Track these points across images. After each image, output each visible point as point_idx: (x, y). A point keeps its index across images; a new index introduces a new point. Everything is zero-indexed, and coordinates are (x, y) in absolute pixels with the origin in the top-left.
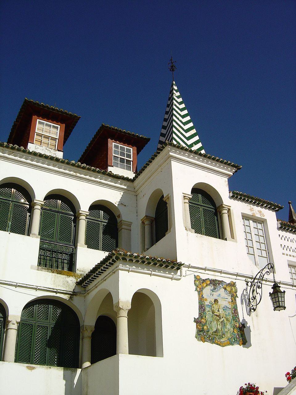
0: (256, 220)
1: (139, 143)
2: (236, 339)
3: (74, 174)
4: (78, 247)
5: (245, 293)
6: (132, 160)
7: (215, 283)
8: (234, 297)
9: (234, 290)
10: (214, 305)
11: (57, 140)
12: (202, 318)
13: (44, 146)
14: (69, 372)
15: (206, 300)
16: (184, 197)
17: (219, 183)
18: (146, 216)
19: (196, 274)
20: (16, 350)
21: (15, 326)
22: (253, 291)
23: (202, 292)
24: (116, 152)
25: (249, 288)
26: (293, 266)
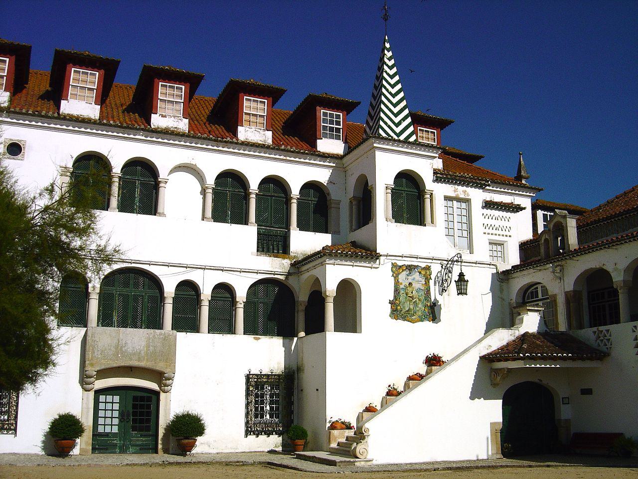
0: (459, 200)
1: (347, 107)
3: (285, 158)
4: (291, 231)
5: (439, 275)
6: (341, 127)
7: (410, 268)
8: (427, 279)
9: (428, 273)
10: (408, 288)
11: (265, 117)
12: (396, 300)
13: (253, 127)
14: (287, 340)
15: (401, 284)
16: (386, 187)
17: (426, 167)
18: (353, 197)
19: (393, 262)
20: (244, 319)
21: (242, 306)
22: (446, 274)
24: (325, 121)
25: (443, 270)
26: (495, 244)
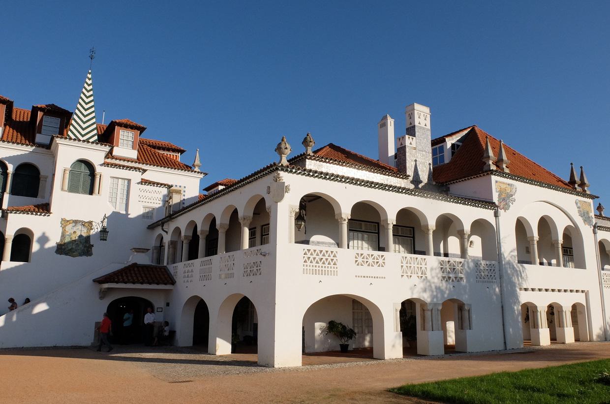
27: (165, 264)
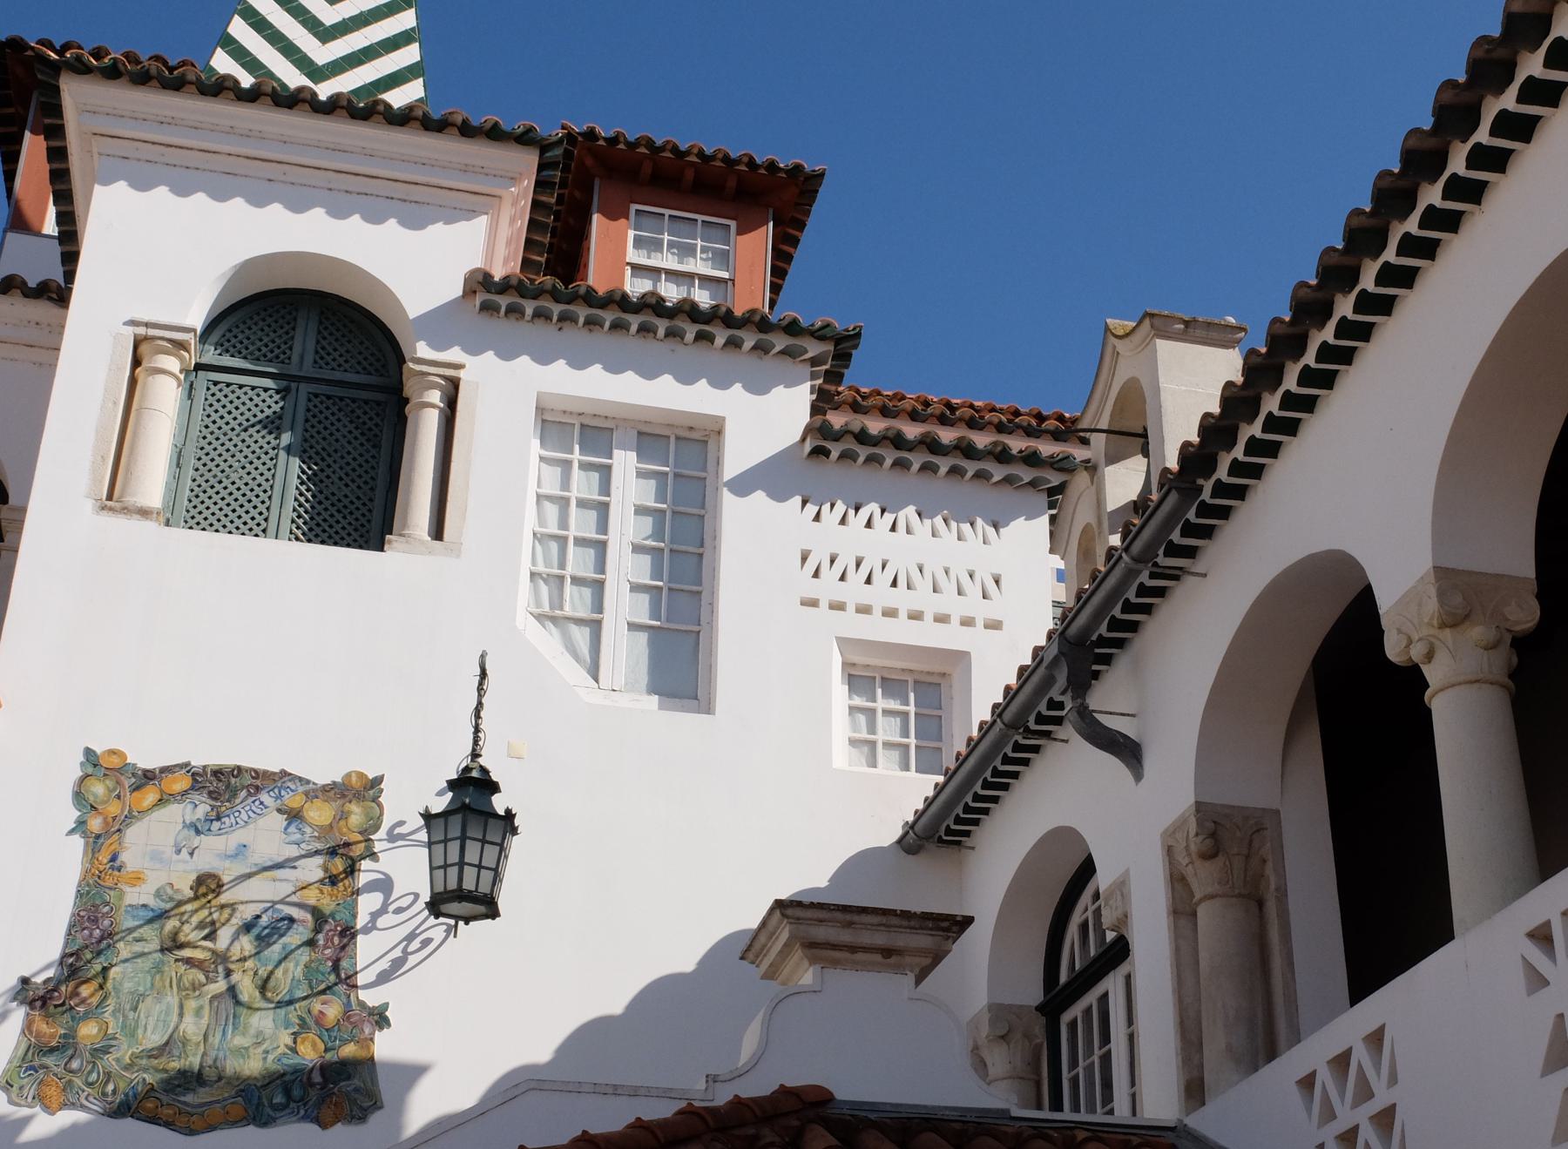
2: (296, 1093)
23: (116, 837)
27: (1159, 1100)
